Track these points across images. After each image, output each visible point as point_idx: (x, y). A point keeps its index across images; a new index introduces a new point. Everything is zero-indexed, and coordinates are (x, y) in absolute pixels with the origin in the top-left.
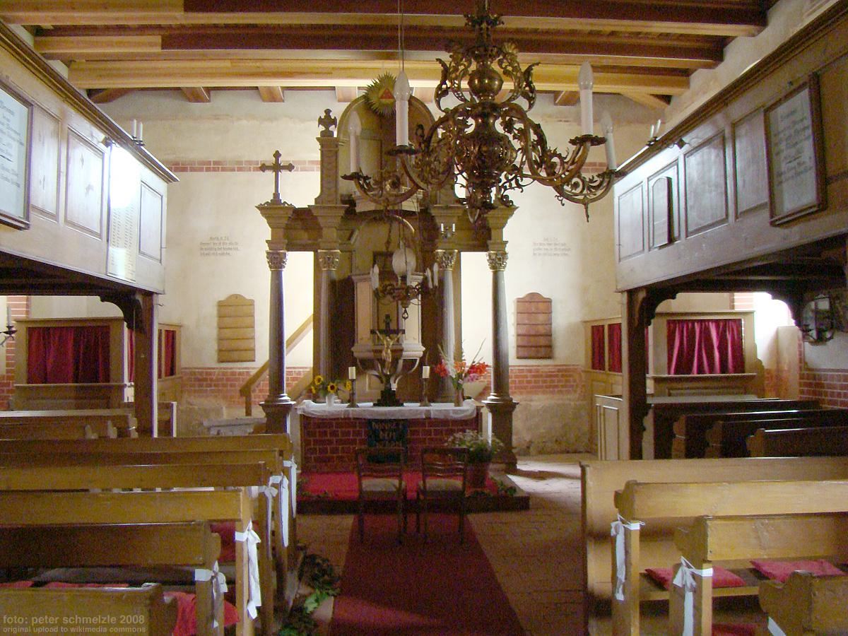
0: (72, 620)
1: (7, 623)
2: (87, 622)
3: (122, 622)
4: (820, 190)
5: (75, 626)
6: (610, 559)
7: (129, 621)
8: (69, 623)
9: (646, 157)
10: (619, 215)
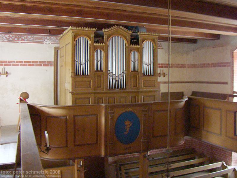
0: (30, 172)
1: (2, 173)
2: (36, 173)
3: (51, 173)
4: (212, 146)
5: (31, 174)
6: (211, 84)
7: (54, 172)
8: (29, 174)
9: (122, 23)
10: (169, 56)
